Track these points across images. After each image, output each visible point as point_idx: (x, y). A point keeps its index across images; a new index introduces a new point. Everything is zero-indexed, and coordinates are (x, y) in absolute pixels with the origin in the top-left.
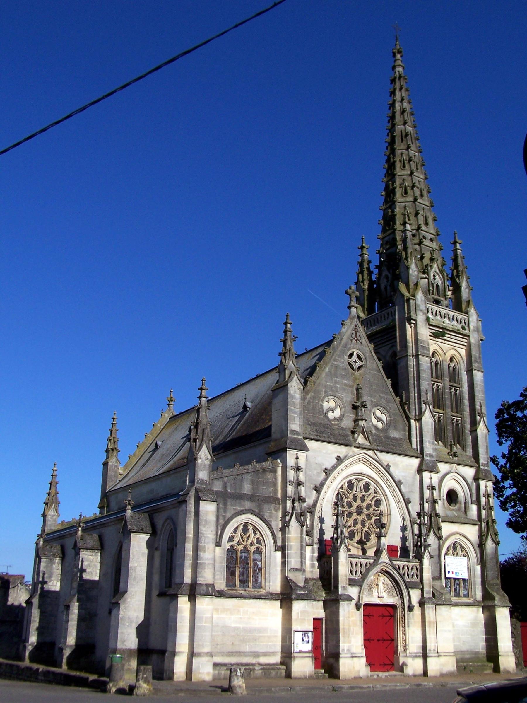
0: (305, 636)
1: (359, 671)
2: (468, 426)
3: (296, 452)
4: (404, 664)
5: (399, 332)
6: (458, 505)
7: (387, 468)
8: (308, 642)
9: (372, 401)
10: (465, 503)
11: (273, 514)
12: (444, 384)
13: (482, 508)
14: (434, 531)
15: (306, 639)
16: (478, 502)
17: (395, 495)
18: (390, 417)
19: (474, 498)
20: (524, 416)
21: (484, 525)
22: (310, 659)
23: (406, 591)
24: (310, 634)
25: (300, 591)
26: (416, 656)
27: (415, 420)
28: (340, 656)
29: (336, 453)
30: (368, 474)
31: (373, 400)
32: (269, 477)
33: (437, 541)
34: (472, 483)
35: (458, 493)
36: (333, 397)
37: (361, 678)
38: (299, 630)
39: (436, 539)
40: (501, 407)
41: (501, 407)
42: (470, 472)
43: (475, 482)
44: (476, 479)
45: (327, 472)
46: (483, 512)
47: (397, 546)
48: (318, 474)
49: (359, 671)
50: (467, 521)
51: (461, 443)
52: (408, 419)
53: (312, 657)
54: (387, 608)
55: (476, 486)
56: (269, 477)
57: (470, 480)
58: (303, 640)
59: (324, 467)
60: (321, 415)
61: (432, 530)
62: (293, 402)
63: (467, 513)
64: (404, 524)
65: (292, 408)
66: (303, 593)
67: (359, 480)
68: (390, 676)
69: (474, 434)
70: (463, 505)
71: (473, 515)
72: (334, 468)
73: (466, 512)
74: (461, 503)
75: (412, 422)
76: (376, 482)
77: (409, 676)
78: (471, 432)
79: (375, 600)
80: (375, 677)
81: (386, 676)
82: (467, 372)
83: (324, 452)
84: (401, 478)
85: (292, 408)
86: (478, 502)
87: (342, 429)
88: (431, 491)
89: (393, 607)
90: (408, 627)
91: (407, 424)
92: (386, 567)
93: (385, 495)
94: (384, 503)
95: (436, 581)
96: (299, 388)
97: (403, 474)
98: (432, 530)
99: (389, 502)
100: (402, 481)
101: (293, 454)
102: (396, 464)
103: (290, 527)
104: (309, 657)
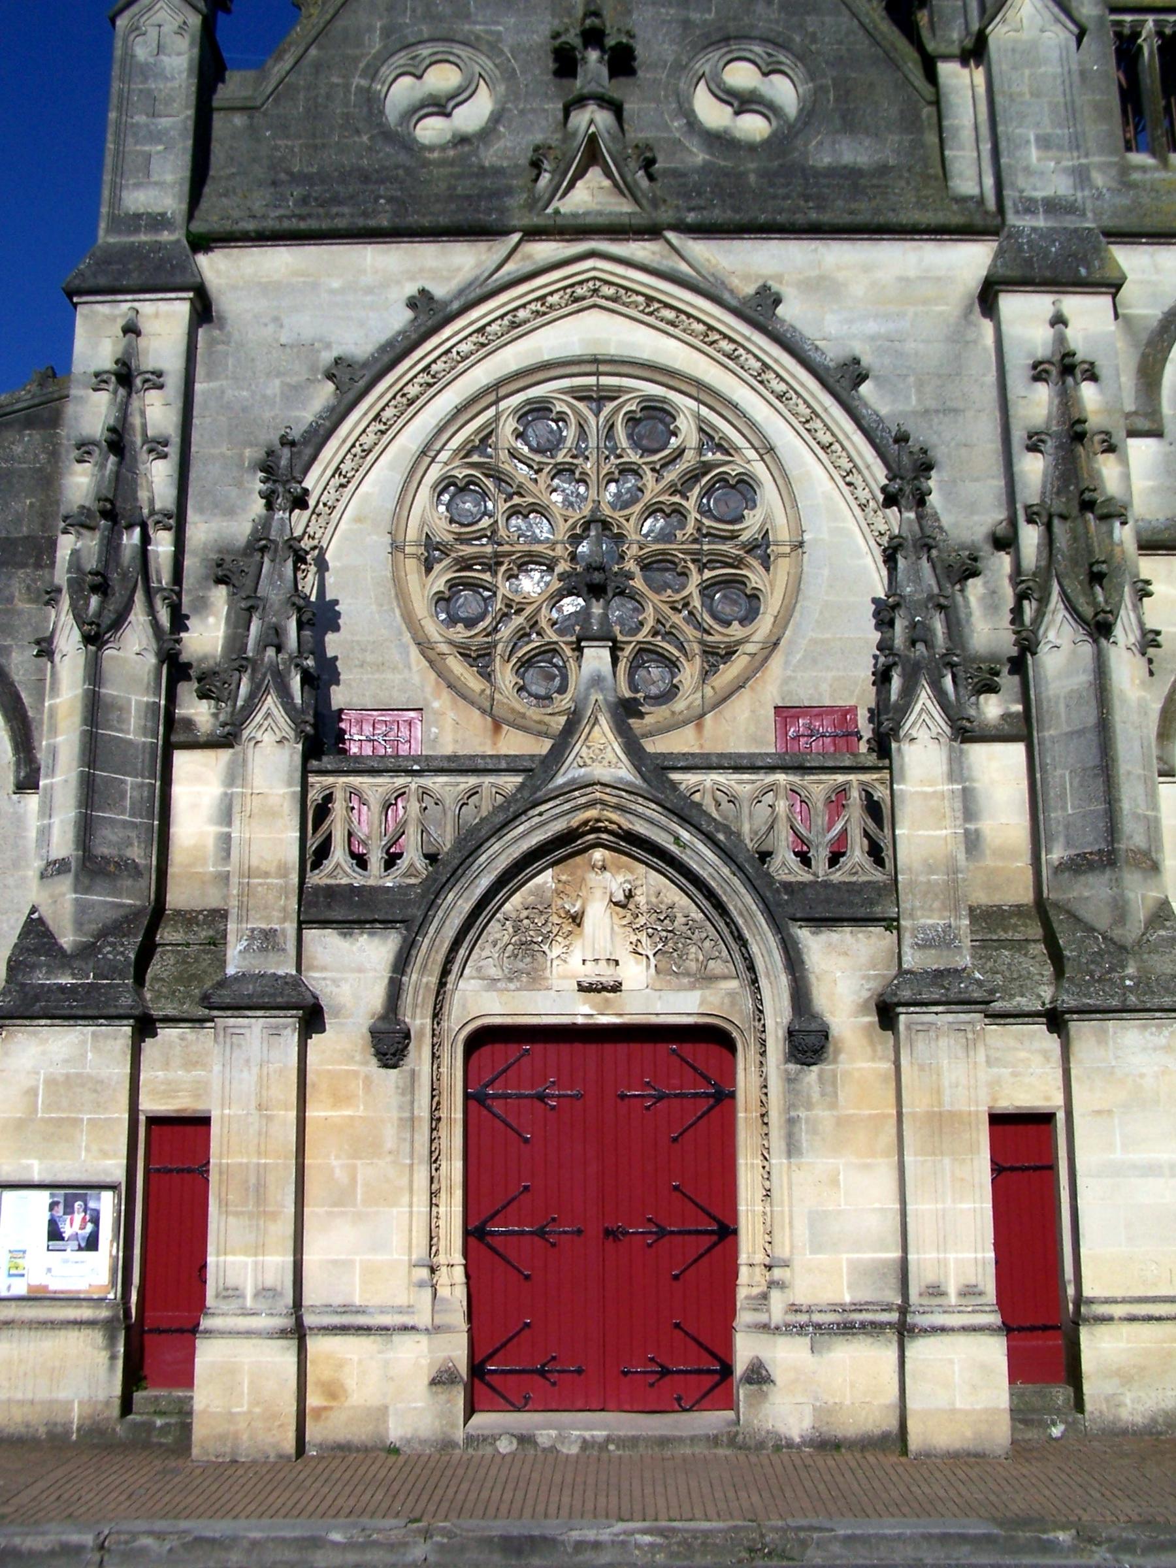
0: (68, 1209)
1: (382, 1412)
3: (121, 308)
4: (759, 1376)
7: (761, 309)
8: (92, 1243)
9: (686, 24)
11: (20, 613)
14: (1064, 594)
15: (73, 1226)
18: (812, 76)
22: (97, 1337)
23: (772, 941)
24: (106, 1204)
25: (50, 973)
26: (847, 1329)
28: (206, 1323)
29: (412, 279)
30: (645, 355)
31: (695, 16)
32: (18, 449)
33: (1087, 649)
36: (440, 47)
37: (393, 1450)
38: (36, 1178)
39: (1081, 634)
45: (352, 379)
47: (853, 710)
48: (295, 393)
49: (382, 1412)
50: (844, 395)
53: (108, 1326)
54: (688, 1049)
56: (18, 449)
58: (55, 1234)
59: (327, 357)
60: (358, 132)
61: (1056, 588)
62: (149, 92)
65: (140, 119)
66: (66, 980)
67: (598, 398)
68: (622, 1442)
72: (396, 352)
76: (701, 390)
77: (783, 1445)
79: (556, 1002)
80: (505, 1446)
81: (585, 1445)
83: (336, 284)
84: (859, 348)
85: (140, 119)
87: (483, 172)
89: (713, 1038)
90: (792, 1149)
92: (618, 808)
93: (767, 450)
94: (769, 493)
95: (1091, 878)
96: (182, 29)
97: (872, 327)
98: (1056, 588)
100: (867, 360)
101: (112, 319)
102: (822, 287)
103: (57, 658)
104: (91, 1323)
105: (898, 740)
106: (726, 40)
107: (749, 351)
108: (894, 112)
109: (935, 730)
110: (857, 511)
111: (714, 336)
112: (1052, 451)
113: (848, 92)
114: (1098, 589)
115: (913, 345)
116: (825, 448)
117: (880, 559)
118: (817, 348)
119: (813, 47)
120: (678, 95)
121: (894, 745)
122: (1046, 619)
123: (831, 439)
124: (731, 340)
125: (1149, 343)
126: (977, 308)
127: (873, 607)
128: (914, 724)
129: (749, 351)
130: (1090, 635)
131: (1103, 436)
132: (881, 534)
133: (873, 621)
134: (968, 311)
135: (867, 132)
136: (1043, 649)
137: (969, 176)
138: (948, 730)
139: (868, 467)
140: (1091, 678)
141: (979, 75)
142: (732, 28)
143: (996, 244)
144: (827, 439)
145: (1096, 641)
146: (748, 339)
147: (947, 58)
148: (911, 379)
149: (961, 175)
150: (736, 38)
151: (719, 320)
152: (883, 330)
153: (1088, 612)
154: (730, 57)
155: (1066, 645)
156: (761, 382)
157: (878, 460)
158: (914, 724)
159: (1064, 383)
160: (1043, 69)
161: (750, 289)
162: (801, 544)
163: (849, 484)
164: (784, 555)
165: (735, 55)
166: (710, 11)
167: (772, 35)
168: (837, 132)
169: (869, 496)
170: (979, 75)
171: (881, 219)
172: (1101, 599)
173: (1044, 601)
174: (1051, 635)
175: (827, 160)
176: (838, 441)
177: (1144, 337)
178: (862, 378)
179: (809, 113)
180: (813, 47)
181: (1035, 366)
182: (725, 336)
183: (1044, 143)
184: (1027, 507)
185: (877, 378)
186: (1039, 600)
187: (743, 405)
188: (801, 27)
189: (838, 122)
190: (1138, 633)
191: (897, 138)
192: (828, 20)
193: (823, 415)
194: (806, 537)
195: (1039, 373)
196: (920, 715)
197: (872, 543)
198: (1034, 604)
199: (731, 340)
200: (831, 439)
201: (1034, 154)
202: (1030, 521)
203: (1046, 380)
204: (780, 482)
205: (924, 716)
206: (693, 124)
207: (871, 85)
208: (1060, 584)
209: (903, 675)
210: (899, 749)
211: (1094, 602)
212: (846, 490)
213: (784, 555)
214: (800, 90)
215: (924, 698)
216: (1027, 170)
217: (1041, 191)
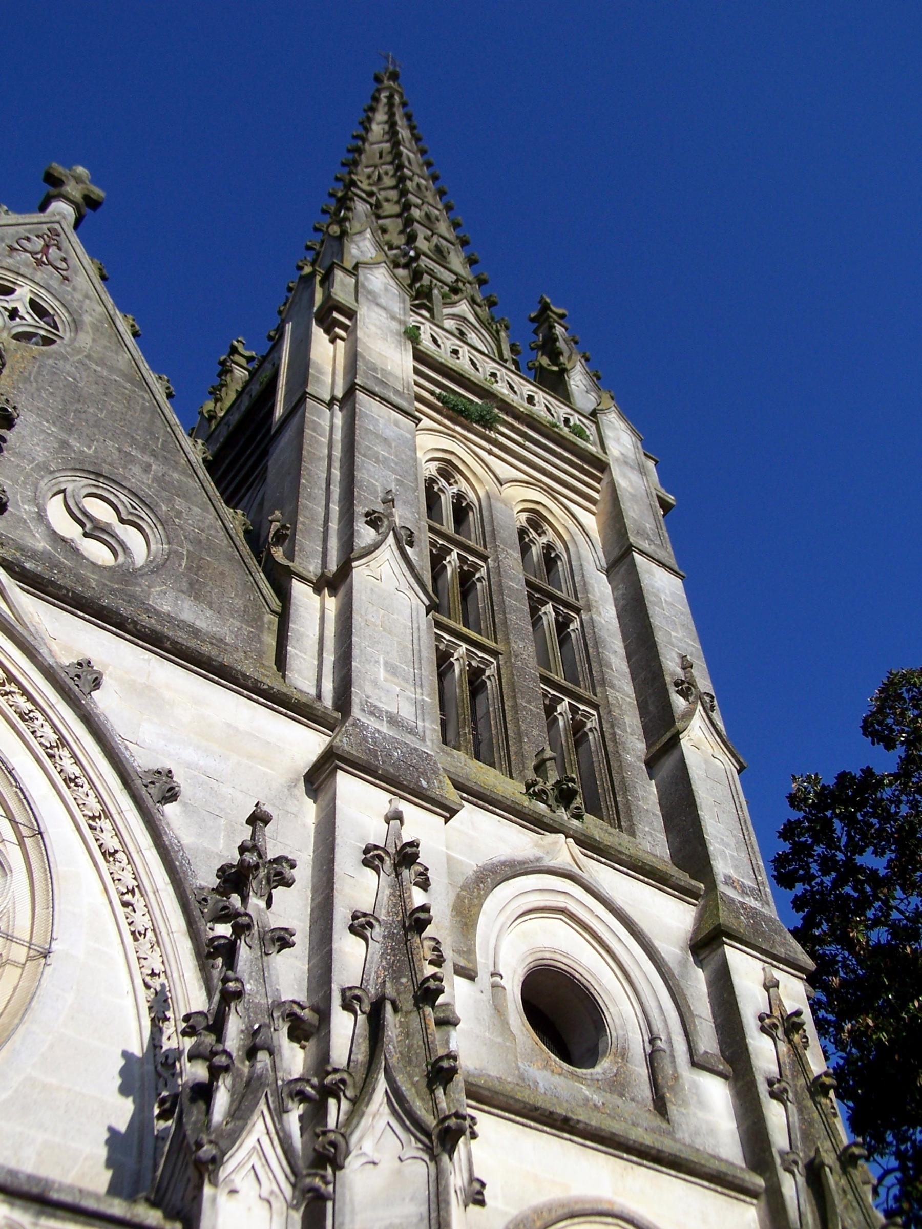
2: (634, 746)
5: (280, 359)
6: (604, 1066)
7: (77, 685)
9: (64, 444)
10: (652, 1059)
12: (497, 559)
13: (763, 1089)
16: (735, 1062)
17: (73, 770)
19: (708, 1041)
20: (920, 756)
21: (791, 1187)
27: (318, 590)
33: (418, 1171)
34: (683, 964)
35: (604, 999)
39: (413, 1148)
40: (801, 914)
41: (801, 914)
42: (671, 918)
43: (699, 963)
44: (706, 943)
46: (776, 1116)
51: (606, 804)
52: (281, 580)
55: (710, 984)
57: (673, 949)
61: (382, 1085)
63: (672, 1109)
64: (155, 1042)
69: (667, 765)
70: (641, 1071)
71: (712, 1132)
73: (660, 1106)
74: (623, 1054)
75: (300, 591)
78: (651, 763)
82: (608, 572)
86: (735, 1062)
88: (386, 879)
91: (276, 604)
98: (382, 1085)
99: (52, 905)
105: (215, 1184)
106: (99, 475)
107: (48, 718)
108: (239, 603)
109: (268, 1186)
110: (129, 938)
111: (13, 688)
112: (380, 939)
113: (199, 568)
114: (440, 1092)
115: (231, 790)
116: (109, 855)
117: (144, 1007)
118: (126, 748)
119: (177, 520)
120: (36, 488)
121: (207, 1190)
122: (363, 1123)
123: (118, 847)
124: (31, 699)
125: (464, 887)
126: (302, 784)
127: (122, 1062)
128: (240, 1166)
129: (48, 718)
130: (429, 1150)
131: (433, 943)
132: (153, 974)
133: (118, 1081)
134: (293, 785)
135: (210, 605)
136: (353, 1164)
137: (306, 674)
138: (288, 1190)
139: (156, 892)
140: (424, 1209)
141: (332, 604)
142: (105, 469)
143: (328, 739)
144: (112, 844)
145: (434, 1158)
146: (52, 706)
147: (303, 579)
148: (223, 822)
149: (299, 672)
150: (106, 478)
151: (24, 673)
152: (201, 763)
153: (431, 1121)
154: (94, 490)
155: (388, 1161)
156: (51, 756)
157: (170, 889)
158: (240, 1166)
159: (398, 875)
160: (395, 616)
161: (66, 660)
162: (46, 954)
163: (126, 904)
164: (15, 964)
165: (100, 492)
166: (89, 447)
167: (141, 493)
168: (182, 591)
169: (149, 925)
170: (332, 604)
171: (226, 660)
172: (443, 1104)
173: (359, 1102)
174: (368, 1146)
175: (166, 608)
176: (126, 851)
177: (460, 881)
178: (171, 795)
179: (156, 568)
180: (177, 520)
181: (366, 851)
182: (25, 693)
183: (392, 670)
184: (343, 991)
185: (185, 805)
186: (354, 1102)
187: (20, 772)
188: (170, 501)
189: (185, 585)
190: (466, 1176)
191: (238, 624)
192: (196, 510)
193: (116, 817)
194: (55, 946)
195: (371, 858)
196: (250, 1155)
197: (139, 982)
198: (345, 1105)
199: (31, 699)
200: (118, 847)
201: (382, 674)
202: (347, 1006)
203: (376, 869)
204: (37, 875)
205: (255, 1160)
206: (41, 517)
207: (222, 573)
208: (390, 1080)
209: (232, 1091)
210: (214, 1199)
211: (435, 1108)
212: (120, 910)
213: (15, 964)
214: (153, 547)
215: (259, 1131)
216: (375, 682)
217: (387, 705)
